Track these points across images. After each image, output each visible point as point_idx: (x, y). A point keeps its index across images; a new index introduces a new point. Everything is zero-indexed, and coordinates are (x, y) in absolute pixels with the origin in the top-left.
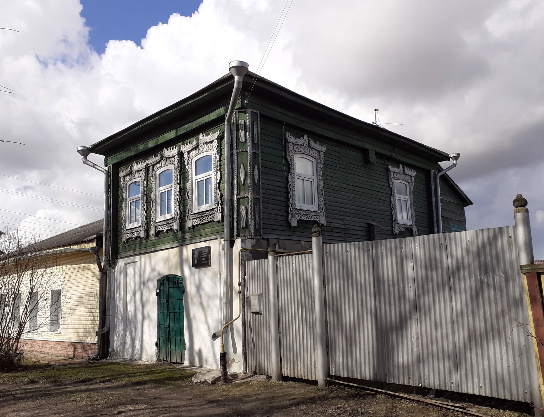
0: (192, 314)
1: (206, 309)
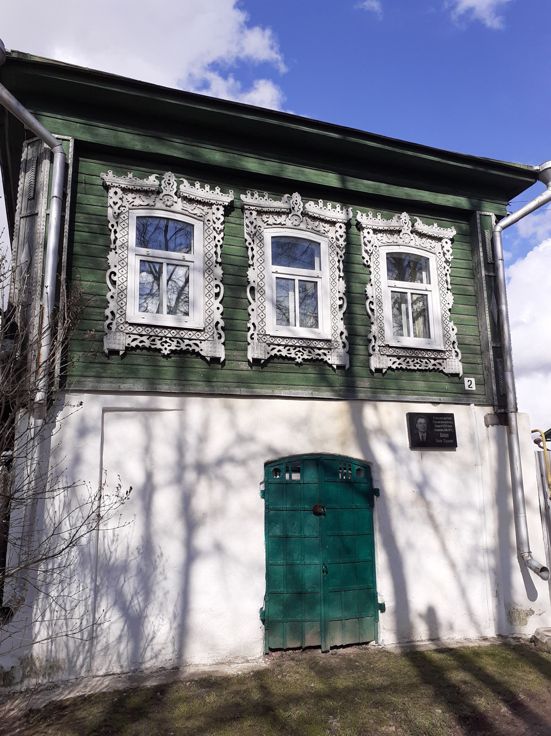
0: (401, 540)
1: (443, 528)
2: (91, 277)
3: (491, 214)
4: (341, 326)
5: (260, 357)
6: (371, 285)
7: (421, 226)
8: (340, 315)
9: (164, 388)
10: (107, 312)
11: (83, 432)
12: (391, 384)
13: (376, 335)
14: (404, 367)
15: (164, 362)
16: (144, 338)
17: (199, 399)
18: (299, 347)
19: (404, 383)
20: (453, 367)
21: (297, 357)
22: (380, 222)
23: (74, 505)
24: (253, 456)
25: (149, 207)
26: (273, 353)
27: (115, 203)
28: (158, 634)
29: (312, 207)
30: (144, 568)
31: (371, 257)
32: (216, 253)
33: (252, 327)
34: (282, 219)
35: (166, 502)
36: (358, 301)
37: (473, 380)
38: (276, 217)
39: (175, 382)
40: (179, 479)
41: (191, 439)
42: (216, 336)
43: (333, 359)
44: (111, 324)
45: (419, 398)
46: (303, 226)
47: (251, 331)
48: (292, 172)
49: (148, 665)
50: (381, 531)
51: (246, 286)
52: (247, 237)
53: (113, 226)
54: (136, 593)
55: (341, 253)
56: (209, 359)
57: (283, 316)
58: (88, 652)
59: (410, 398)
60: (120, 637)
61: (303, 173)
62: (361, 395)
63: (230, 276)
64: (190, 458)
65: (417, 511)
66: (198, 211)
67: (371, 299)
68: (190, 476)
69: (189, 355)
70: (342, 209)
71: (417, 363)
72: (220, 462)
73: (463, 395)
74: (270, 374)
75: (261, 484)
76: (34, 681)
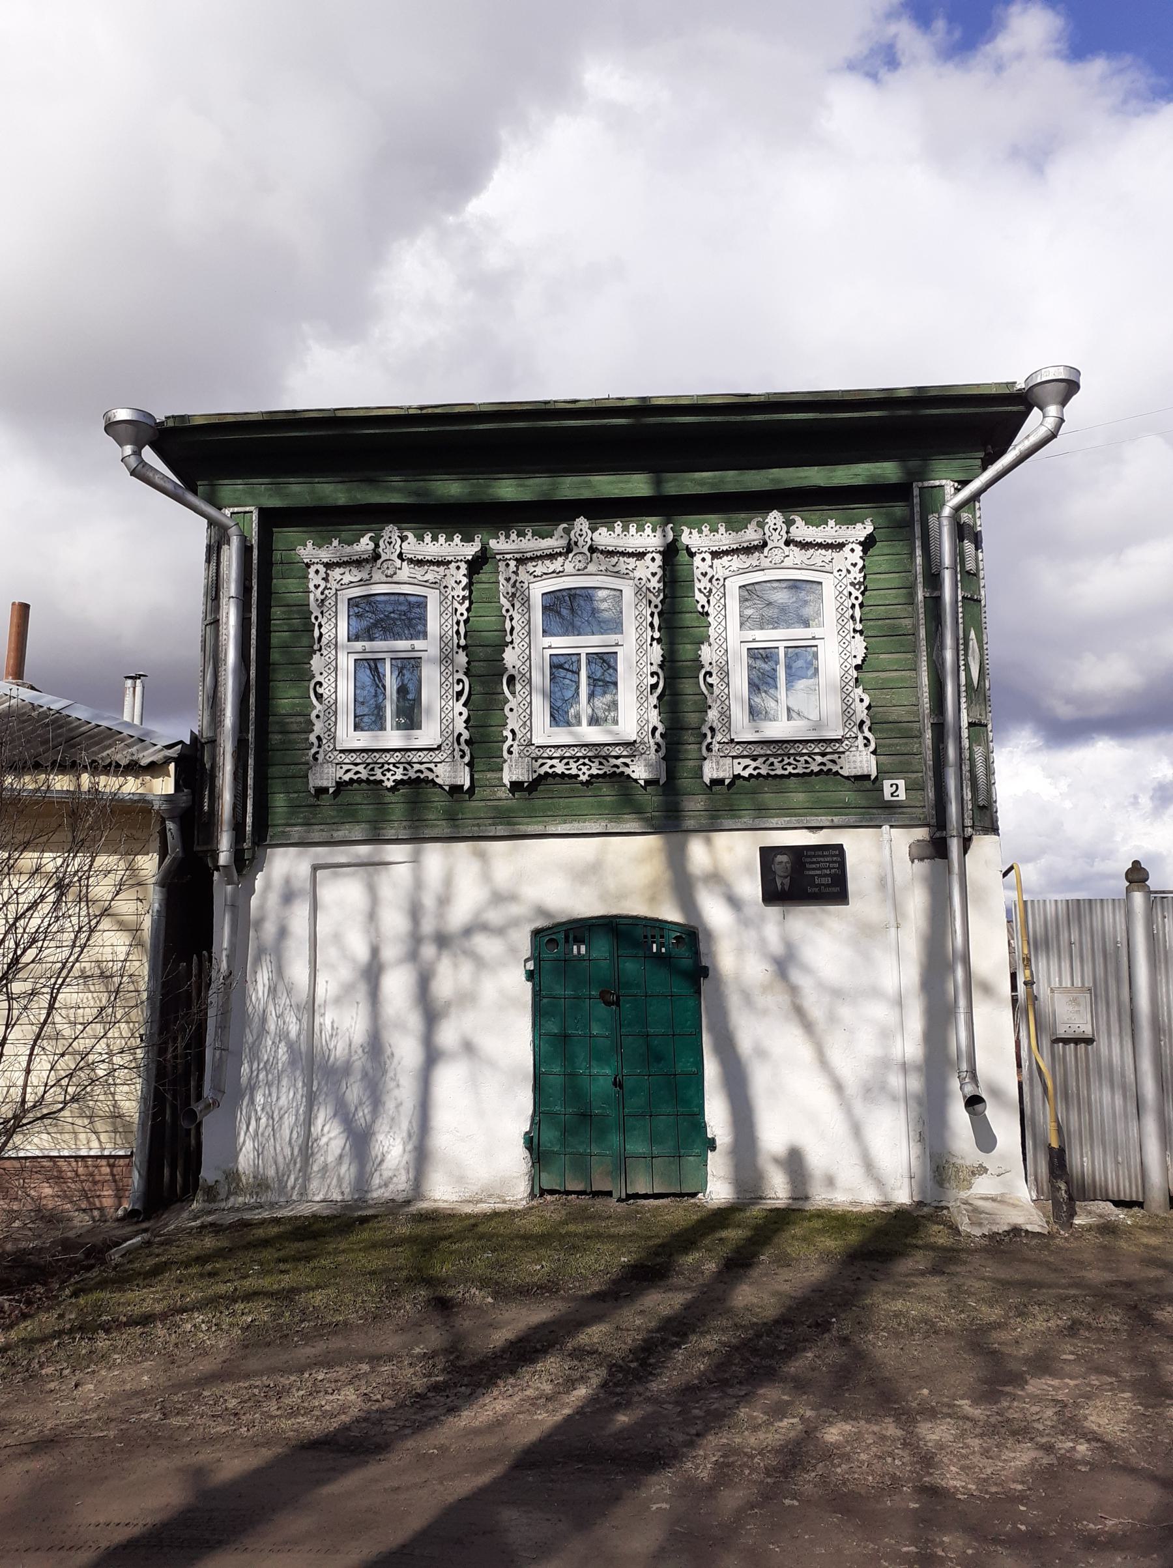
0: (745, 1042)
2: (293, 692)
3: (943, 482)
4: (654, 718)
5: (521, 779)
6: (710, 645)
7: (802, 531)
8: (653, 700)
9: (390, 834)
10: (312, 738)
11: (288, 897)
12: (745, 802)
13: (714, 725)
14: (763, 772)
15: (390, 797)
16: (360, 768)
17: (438, 845)
18: (584, 758)
19: (769, 798)
20: (858, 764)
21: (580, 773)
22: (724, 539)
23: (280, 987)
24: (515, 923)
25: (363, 582)
26: (542, 771)
27: (317, 587)
28: (389, 1157)
29: (605, 537)
30: (371, 1072)
31: (711, 598)
32: (458, 632)
33: (510, 736)
34: (557, 565)
35: (397, 985)
36: (687, 674)
37: (901, 783)
38: (547, 562)
39: (404, 823)
40: (413, 956)
41: (429, 901)
42: (457, 754)
43: (639, 771)
44: (317, 753)
45: (794, 821)
46: (592, 568)
47: (509, 742)
48: (570, 487)
49: (375, 1195)
50: (711, 1030)
51: (502, 675)
52: (503, 601)
53: (316, 618)
54: (361, 1103)
55: (657, 601)
56: (447, 788)
57: (559, 716)
58: (300, 1171)
59: (774, 822)
60: (341, 1156)
61: (589, 485)
62: (690, 823)
63: (481, 663)
64: (428, 926)
65: (776, 1000)
66: (430, 577)
67: (708, 668)
68: (428, 951)
69: (423, 784)
70: (654, 530)
71: (789, 764)
72: (467, 932)
73: (880, 811)
74: (543, 800)
75: (526, 961)
76: (241, 1199)
